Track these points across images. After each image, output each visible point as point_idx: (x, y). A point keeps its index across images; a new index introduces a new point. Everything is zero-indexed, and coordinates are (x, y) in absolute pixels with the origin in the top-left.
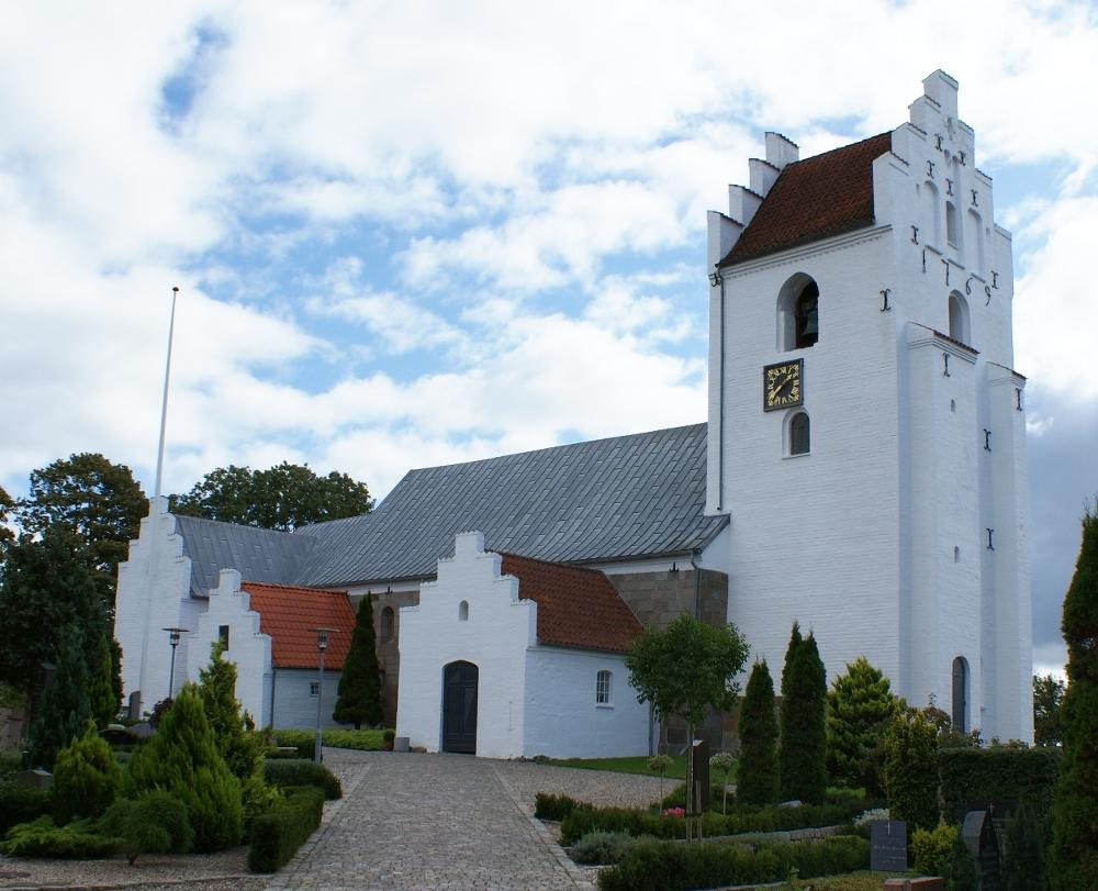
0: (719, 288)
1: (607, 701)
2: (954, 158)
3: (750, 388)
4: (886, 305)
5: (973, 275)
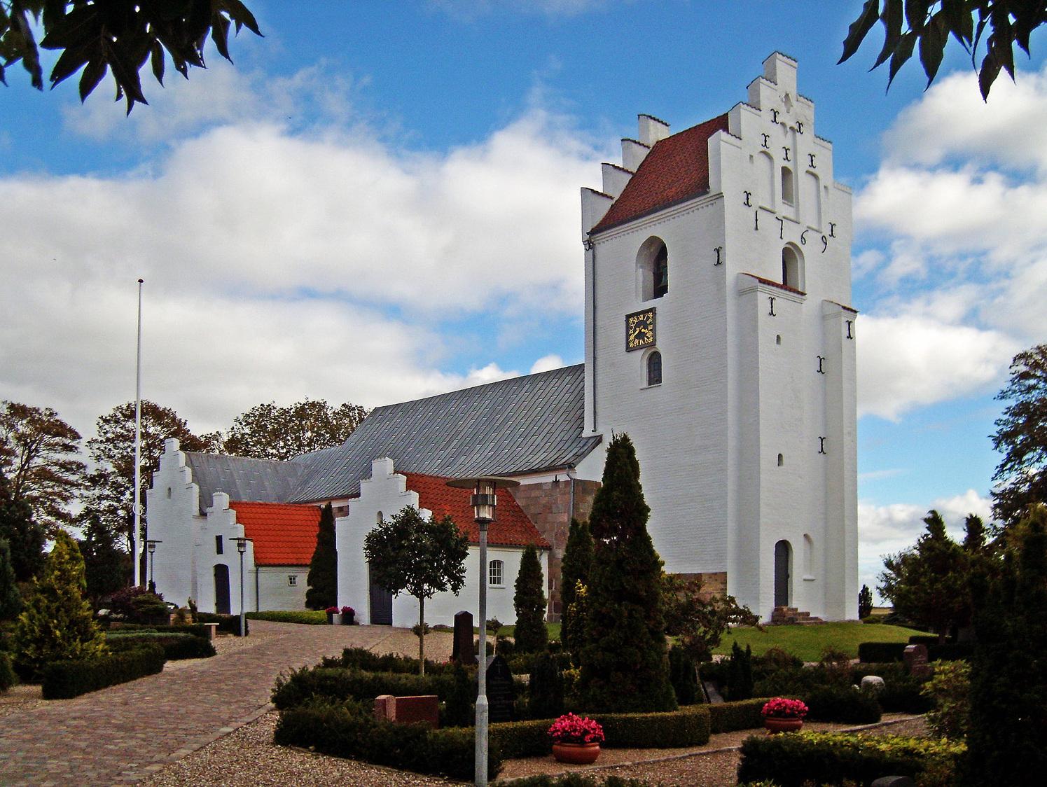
0: (591, 251)
1: (499, 583)
2: (792, 128)
3: (615, 333)
4: (718, 259)
5: (808, 227)
